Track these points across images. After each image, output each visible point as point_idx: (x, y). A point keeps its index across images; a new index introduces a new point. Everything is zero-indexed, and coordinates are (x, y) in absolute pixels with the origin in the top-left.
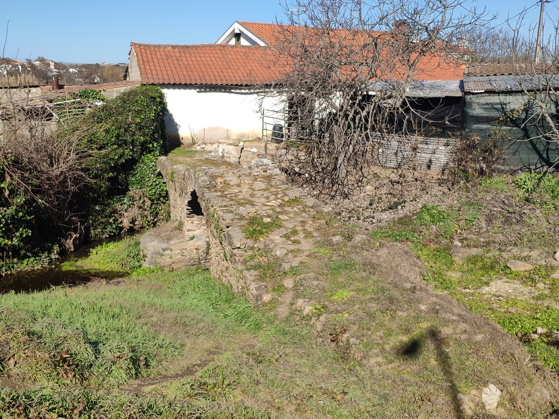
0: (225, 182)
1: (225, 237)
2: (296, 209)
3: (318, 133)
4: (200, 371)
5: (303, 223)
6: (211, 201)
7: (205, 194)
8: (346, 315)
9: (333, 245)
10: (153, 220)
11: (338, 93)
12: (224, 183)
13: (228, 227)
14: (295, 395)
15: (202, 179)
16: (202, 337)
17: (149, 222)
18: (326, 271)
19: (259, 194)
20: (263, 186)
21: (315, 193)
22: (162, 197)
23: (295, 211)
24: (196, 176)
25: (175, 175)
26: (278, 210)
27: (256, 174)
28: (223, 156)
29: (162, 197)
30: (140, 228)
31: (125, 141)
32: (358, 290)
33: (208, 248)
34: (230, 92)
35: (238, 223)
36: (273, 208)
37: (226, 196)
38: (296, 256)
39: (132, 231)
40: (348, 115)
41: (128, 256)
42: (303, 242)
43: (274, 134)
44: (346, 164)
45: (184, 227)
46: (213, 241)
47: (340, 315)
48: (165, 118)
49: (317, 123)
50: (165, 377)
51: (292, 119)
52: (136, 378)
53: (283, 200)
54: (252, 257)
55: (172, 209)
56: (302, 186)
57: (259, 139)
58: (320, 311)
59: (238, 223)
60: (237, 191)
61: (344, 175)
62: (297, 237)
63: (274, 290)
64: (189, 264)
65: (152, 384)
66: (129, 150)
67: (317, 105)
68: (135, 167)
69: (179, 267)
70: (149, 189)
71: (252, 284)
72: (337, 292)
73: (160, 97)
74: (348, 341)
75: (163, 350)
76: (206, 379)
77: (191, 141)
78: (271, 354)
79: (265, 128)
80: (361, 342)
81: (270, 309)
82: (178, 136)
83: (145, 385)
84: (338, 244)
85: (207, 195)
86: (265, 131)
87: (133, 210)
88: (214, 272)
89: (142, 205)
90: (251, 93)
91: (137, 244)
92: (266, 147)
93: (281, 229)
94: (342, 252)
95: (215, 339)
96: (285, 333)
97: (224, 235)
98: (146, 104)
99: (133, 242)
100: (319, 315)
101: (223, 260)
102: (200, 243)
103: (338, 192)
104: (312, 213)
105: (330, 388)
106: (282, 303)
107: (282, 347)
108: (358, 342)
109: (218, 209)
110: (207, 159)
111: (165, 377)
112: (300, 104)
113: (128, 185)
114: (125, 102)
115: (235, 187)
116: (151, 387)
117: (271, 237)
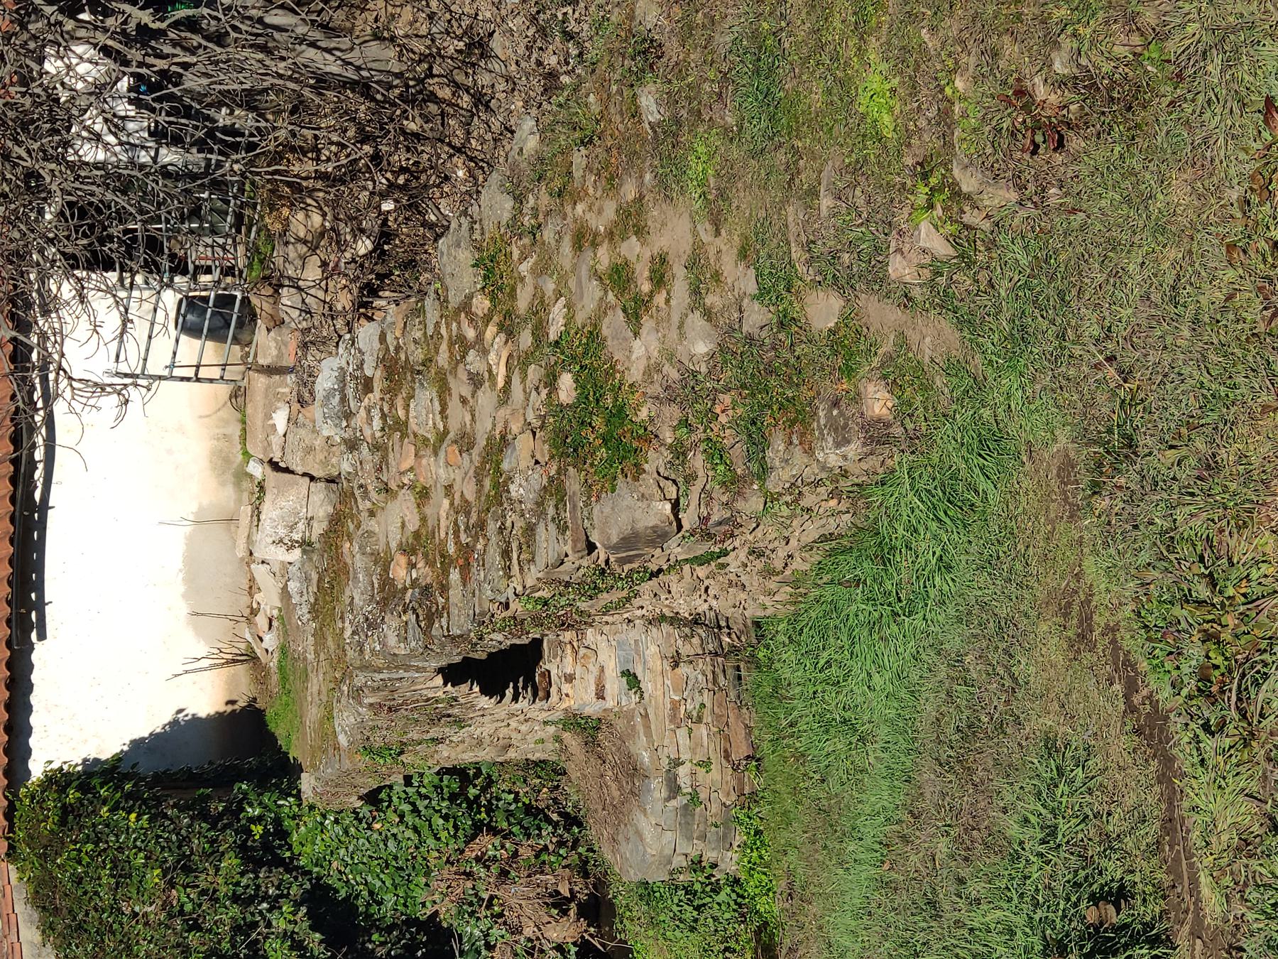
0: (407, 551)
1: (629, 560)
2: (524, 268)
3: (214, 157)
4: (1153, 686)
5: (583, 239)
6: (483, 603)
7: (456, 631)
8: (959, 84)
9: (678, 122)
10: (556, 825)
11: (47, 66)
12: (413, 551)
13: (591, 547)
14: (1268, 313)
15: (392, 640)
16: (1024, 667)
17: (561, 844)
18: (781, 157)
19: (458, 416)
20: (425, 397)
21: (460, 173)
22: (463, 789)
23: (533, 271)
24: (380, 662)
25: (377, 742)
26: (526, 339)
27: (377, 423)
28: (305, 544)
29: (463, 789)
30: (586, 875)
31: (237, 929)
32: (861, 29)
33: (675, 620)
34: (44, 506)
35: (574, 507)
36: (517, 363)
37: (466, 551)
38: (717, 276)
39: (597, 909)
40: (142, 28)
41: (692, 929)
42: (660, 242)
43: (216, 334)
44: (345, 43)
45: (588, 711)
46: (646, 603)
47: (957, 109)
48: (146, 768)
49: (169, 156)
50: (1170, 824)
51: (154, 257)
52: (1170, 943)
53: (487, 319)
54: (716, 452)
55: (512, 754)
56: (431, 226)
57: (238, 395)
58: (941, 191)
59: (574, 507)
60: (446, 503)
61: (392, 53)
62: (638, 267)
63: (849, 371)
64: (732, 695)
65: (1194, 882)
66: (273, 917)
67: (92, 153)
68: (343, 894)
69: (742, 733)
70: (431, 842)
71: (820, 456)
72: (863, 117)
73: (63, 790)
74: (1061, 83)
75: (1063, 827)
76: (1185, 669)
77: (240, 668)
78: (1101, 398)
79: (190, 373)
80: (1070, 30)
81: (925, 388)
82: (219, 719)
83: (1198, 910)
84: (671, 100)
85: (459, 622)
86: (203, 373)
87: (513, 902)
88: (767, 601)
89: (495, 869)
90: (50, 422)
91: (646, 891)
92: (270, 370)
93: (605, 331)
94: (706, 87)
95: (1033, 613)
96: (1021, 336)
97: (622, 562)
98: (90, 847)
99: (640, 909)
100: (957, 194)
101: (724, 566)
102: (653, 649)
103: (460, 78)
104: (545, 199)
105: (1250, 168)
106: (903, 342)
107: (1077, 351)
108: (1067, 43)
109: (516, 584)
110: (314, 610)
111: (1170, 824)
112: (91, 227)
113: (411, 922)
114: (79, 927)
115: (428, 510)
116: (1205, 891)
117: (635, 374)
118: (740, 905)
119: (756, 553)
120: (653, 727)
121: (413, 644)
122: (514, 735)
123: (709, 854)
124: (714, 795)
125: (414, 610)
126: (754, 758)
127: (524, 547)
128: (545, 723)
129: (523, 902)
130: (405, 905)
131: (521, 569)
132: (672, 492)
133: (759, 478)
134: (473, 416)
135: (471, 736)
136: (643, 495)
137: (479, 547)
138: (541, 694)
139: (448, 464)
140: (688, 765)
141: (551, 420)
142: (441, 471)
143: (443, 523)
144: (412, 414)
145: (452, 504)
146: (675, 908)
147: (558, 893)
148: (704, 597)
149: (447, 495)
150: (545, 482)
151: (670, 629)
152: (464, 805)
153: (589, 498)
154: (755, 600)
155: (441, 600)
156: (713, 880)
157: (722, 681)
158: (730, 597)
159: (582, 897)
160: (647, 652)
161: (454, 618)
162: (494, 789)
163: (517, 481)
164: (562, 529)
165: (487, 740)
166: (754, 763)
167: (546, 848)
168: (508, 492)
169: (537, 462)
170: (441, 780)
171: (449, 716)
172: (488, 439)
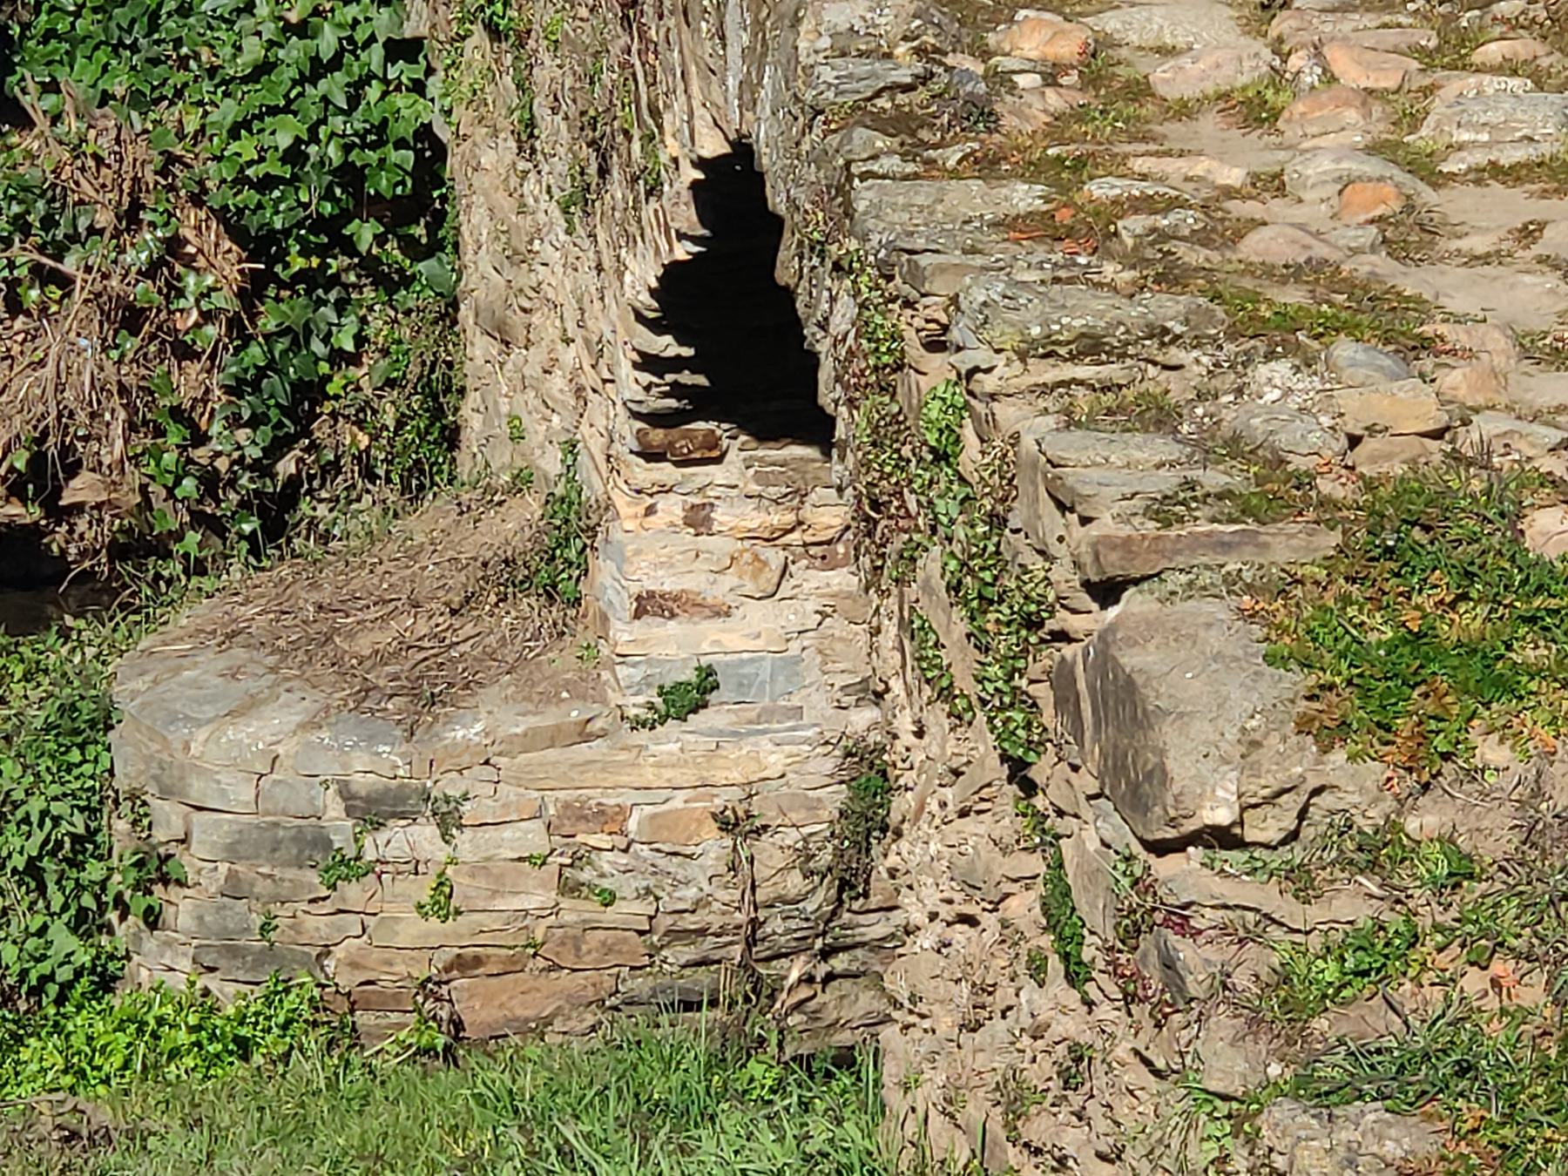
0: (1096, 64)
1: (1066, 700)
6: (940, 277)
7: (864, 197)
10: (263, 468)
12: (1091, 80)
13: (1106, 592)
17: (211, 482)
19: (1485, 215)
30: (117, 552)
35: (1225, 546)
37: (1098, 231)
45: (603, 570)
46: (938, 751)
54: (1375, 959)
55: (479, 348)
59: (1225, 546)
60: (1233, 176)
64: (639, 985)
70: (228, 111)
85: (890, 207)
87: (52, 342)
88: (929, 1093)
89: (144, 292)
97: (1062, 679)
101: (1037, 969)
102: (775, 761)
109: (1004, 374)
115: (1209, 124)
118: (37, 991)
119: (1075, 1066)
120: (552, 754)
121: (828, 74)
122: (537, 356)
123: (185, 906)
124: (353, 924)
125: (925, 79)
126: (454, 1044)
127: (1108, 399)
128: (571, 447)
129: (49, 371)
130: (50, 34)
131: (1046, 389)
132: (1265, 827)
133: (1301, 1082)
134: (1485, 259)
135: (538, 233)
136: (1255, 744)
137: (1110, 269)
138: (657, 436)
139: (1346, 183)
140: (442, 852)
141: (1477, 486)
142: (1325, 164)
143: (1174, 167)
144: (1491, 83)
145: (1229, 193)
146: (35, 806)
147: (73, 470)
148: (946, 912)
149: (1255, 178)
150: (1298, 463)
151: (830, 811)
152: (328, 208)
153: (1249, 588)
154: (932, 1058)
155: (952, 156)
156: (113, 916)
157: (680, 954)
158: (944, 988)
159: (57, 540)
160: (765, 743)
161: (900, 193)
162: (369, 293)
163: (1305, 383)
164: (1163, 510)
165: (525, 279)
166: (441, 1041)
167: (200, 439)
168: (1270, 356)
169: (1354, 441)
170: (401, 144)
171: (603, 172)
172: (1419, 300)
